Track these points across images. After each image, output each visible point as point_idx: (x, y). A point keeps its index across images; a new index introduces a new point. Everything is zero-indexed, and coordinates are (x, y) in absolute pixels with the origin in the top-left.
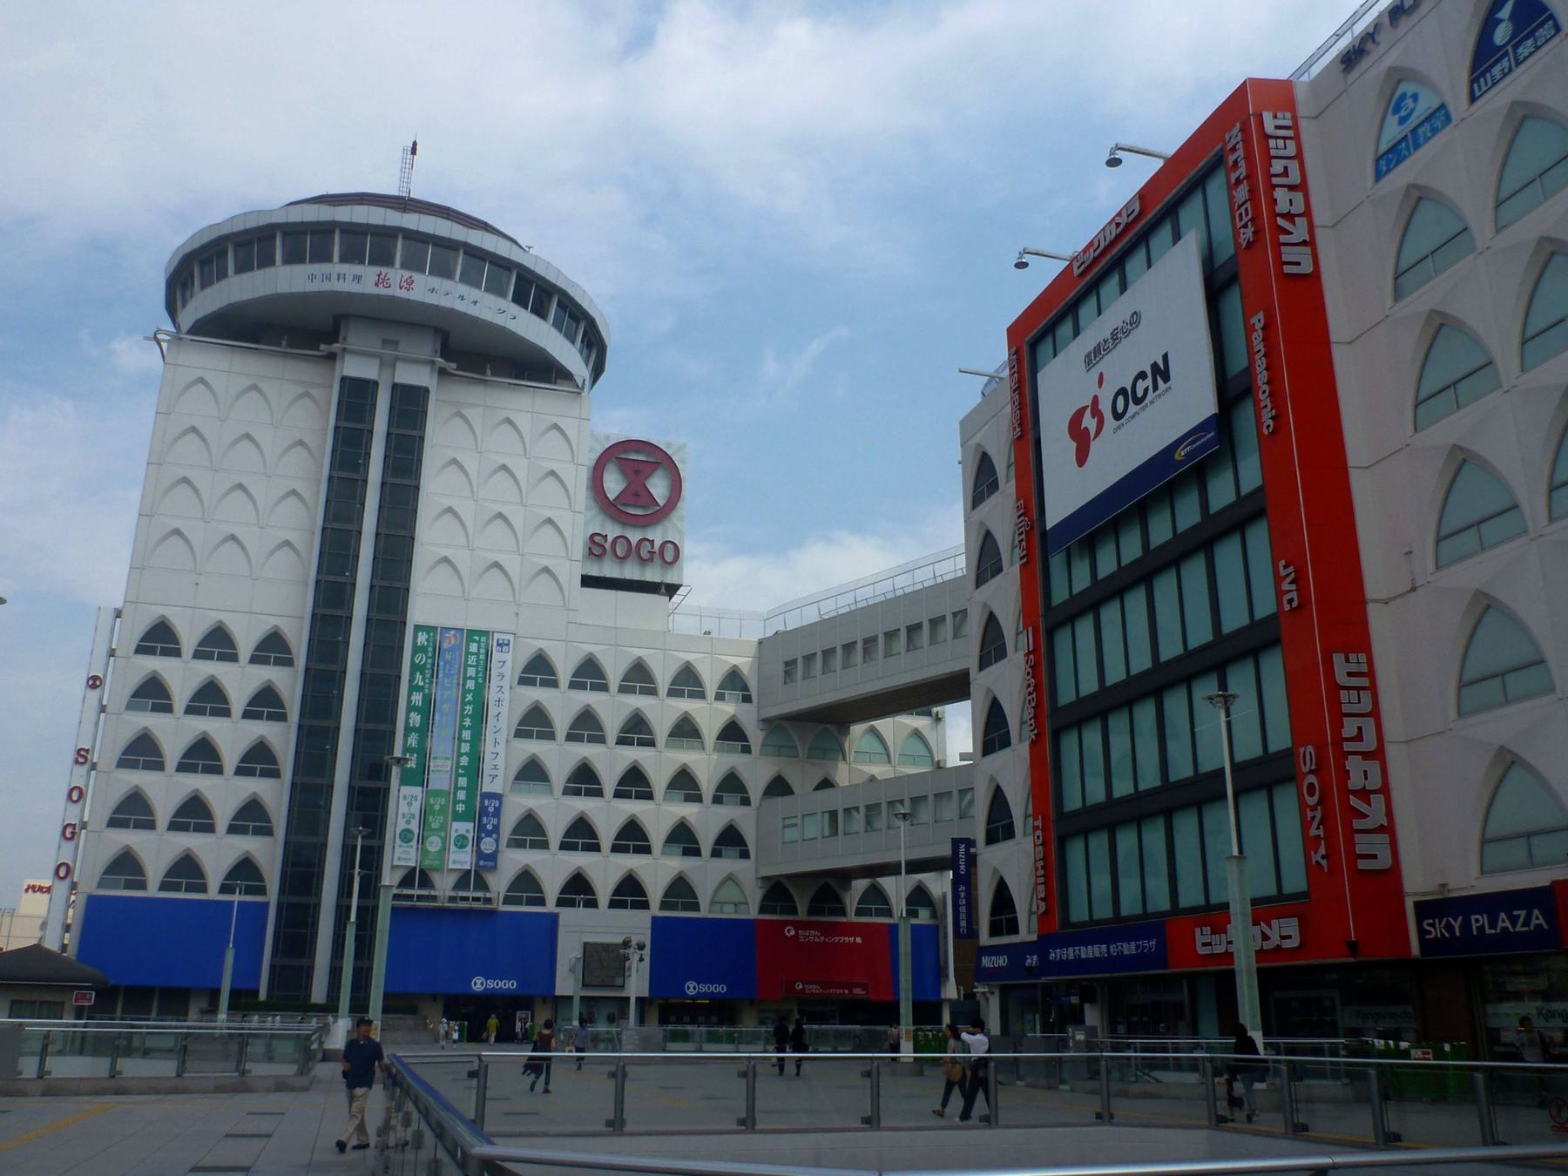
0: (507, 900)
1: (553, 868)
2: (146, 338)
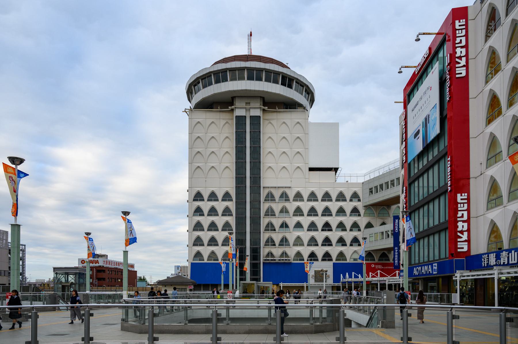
1: (306, 251)
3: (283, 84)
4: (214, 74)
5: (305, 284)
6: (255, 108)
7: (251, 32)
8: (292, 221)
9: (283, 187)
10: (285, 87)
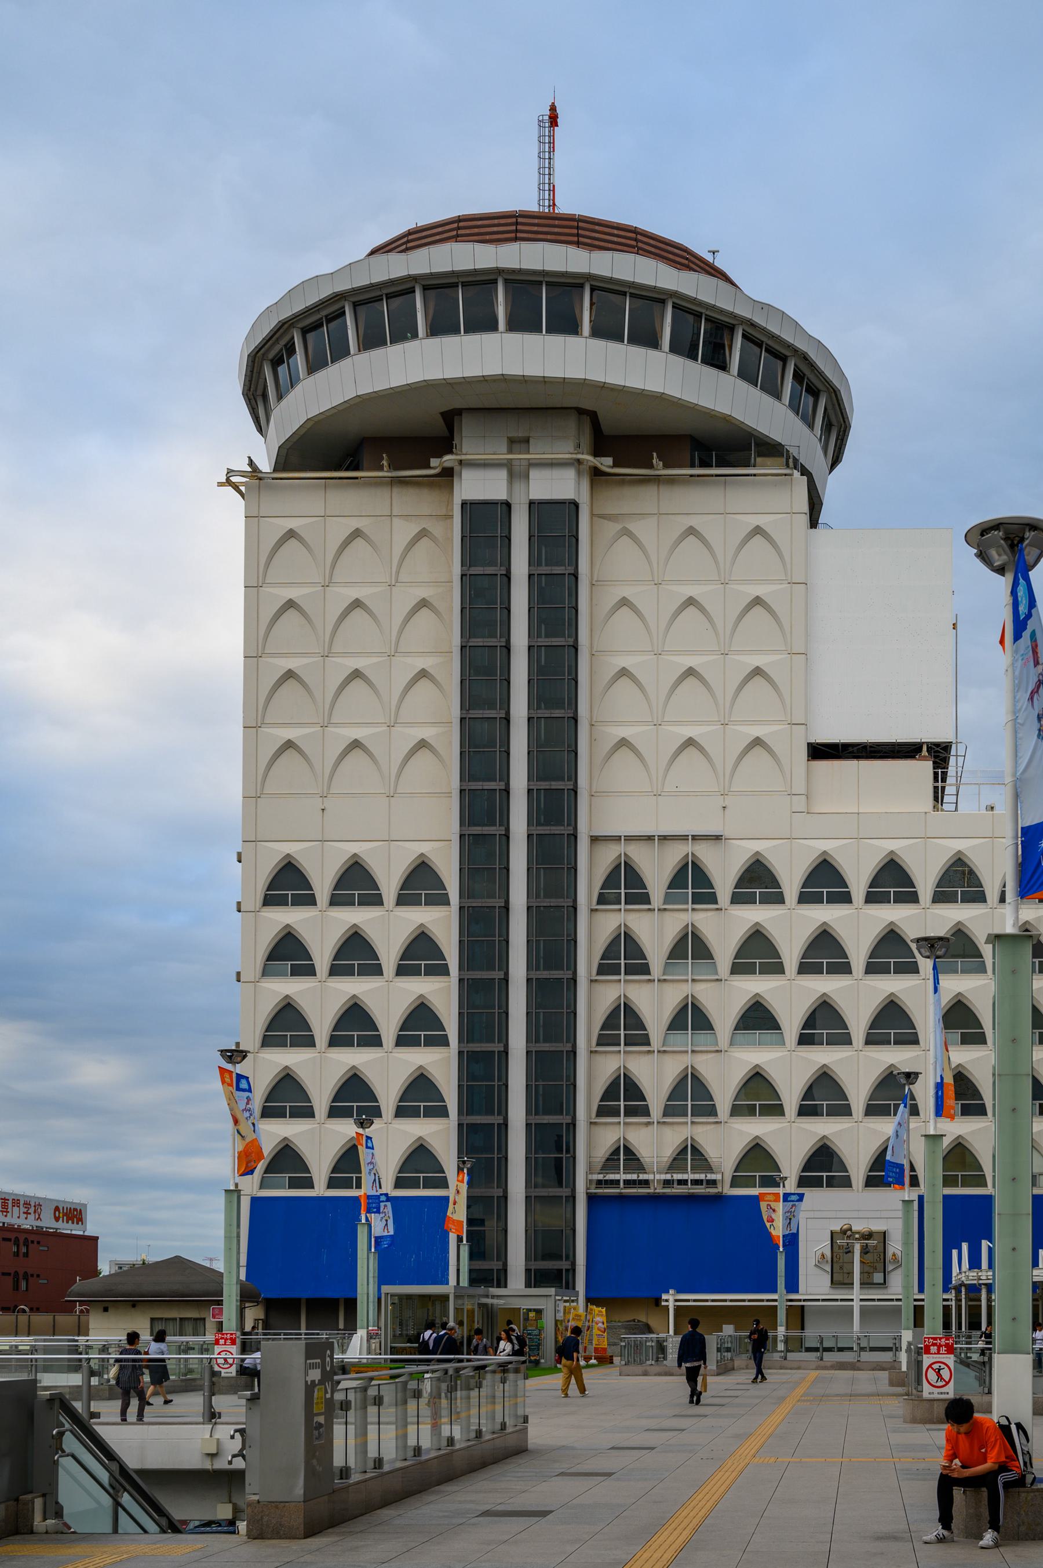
0: (735, 1182)
1: (791, 1140)
2: (220, 484)
3: (684, 348)
4: (355, 305)
5: (778, 1298)
6: (552, 464)
7: (553, 108)
8: (726, 997)
9: (684, 838)
10: (689, 363)
